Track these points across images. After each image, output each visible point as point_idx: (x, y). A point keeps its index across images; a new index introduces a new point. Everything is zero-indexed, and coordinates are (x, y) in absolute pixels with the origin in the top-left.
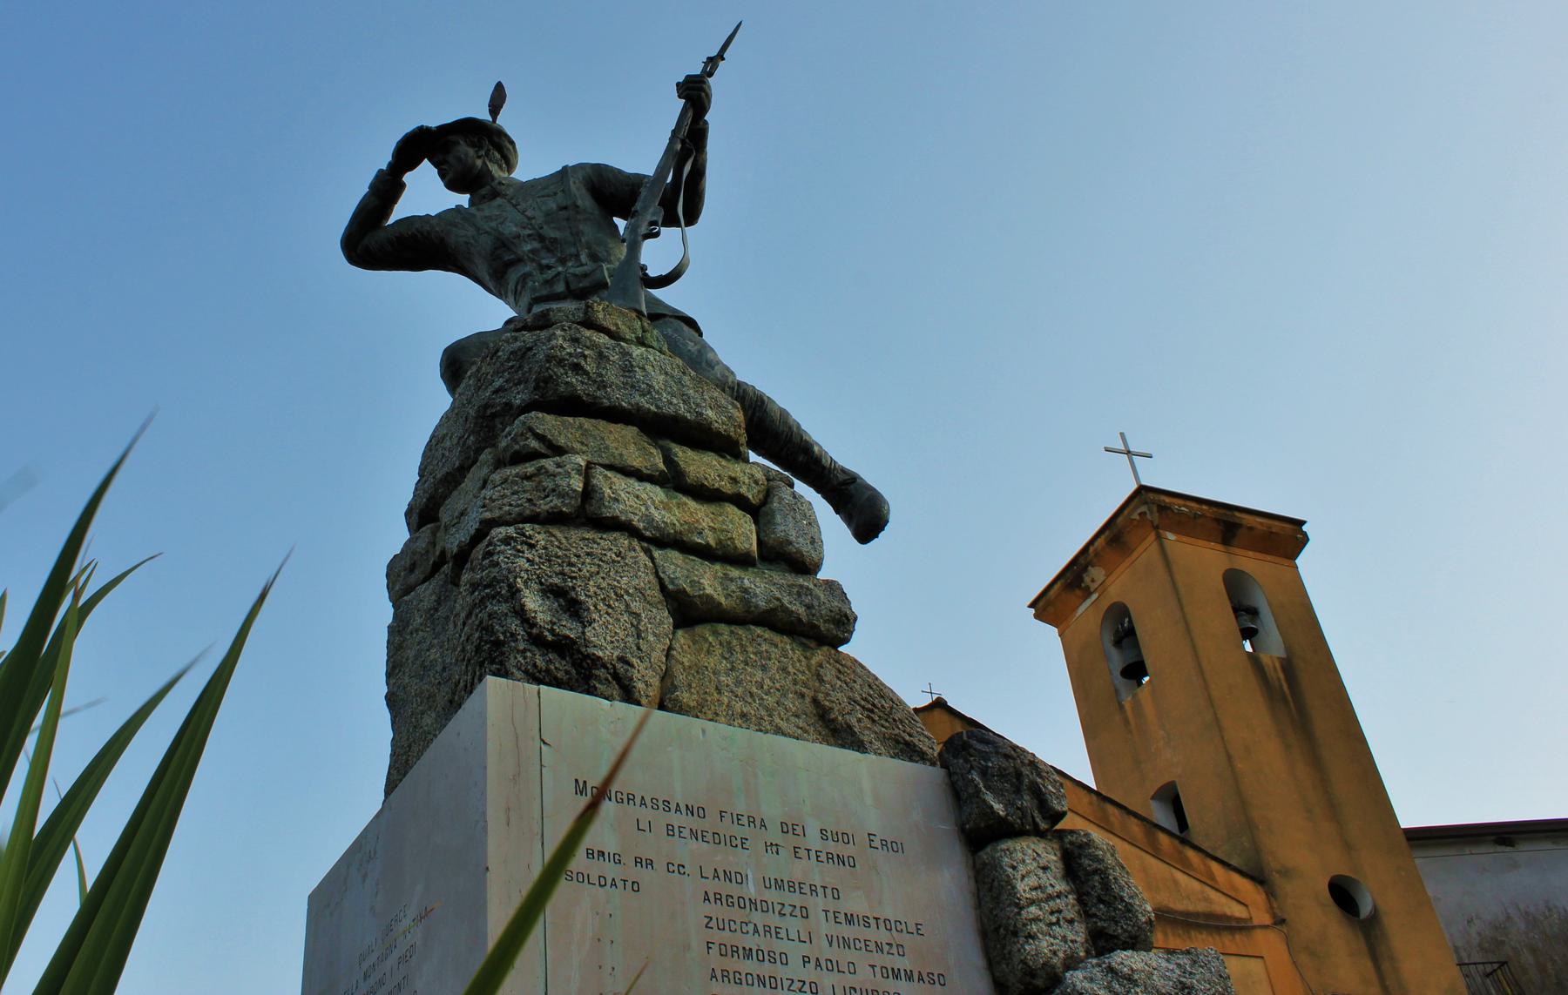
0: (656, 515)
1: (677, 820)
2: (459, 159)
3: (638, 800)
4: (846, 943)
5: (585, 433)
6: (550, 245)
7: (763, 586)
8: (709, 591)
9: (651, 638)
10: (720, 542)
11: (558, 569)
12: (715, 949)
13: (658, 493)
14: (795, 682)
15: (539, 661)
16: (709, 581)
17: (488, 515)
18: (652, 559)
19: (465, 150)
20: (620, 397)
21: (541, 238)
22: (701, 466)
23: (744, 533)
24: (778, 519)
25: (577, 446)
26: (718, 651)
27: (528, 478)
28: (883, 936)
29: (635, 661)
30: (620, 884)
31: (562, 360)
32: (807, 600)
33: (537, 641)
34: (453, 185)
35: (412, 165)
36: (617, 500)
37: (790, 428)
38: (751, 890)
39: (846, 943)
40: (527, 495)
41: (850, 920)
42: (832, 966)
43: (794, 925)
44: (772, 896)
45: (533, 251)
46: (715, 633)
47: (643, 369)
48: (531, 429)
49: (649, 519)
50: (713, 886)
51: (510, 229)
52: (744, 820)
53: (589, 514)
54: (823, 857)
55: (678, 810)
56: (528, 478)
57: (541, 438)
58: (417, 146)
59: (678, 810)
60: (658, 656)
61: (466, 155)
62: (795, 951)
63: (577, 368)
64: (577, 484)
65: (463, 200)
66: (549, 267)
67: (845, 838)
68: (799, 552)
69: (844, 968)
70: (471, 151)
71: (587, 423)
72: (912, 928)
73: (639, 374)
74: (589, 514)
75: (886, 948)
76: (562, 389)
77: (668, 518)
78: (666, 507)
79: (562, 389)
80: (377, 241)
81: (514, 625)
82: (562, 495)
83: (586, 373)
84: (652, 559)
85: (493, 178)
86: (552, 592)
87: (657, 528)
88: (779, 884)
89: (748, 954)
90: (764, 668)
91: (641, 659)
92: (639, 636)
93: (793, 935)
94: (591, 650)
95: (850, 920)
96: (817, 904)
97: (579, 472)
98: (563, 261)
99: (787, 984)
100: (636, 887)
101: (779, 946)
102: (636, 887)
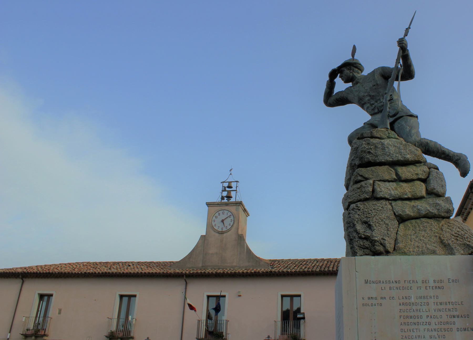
0: (393, 192)
1: (392, 285)
2: (346, 75)
3: (382, 282)
4: (440, 310)
5: (373, 171)
6: (372, 97)
7: (424, 206)
8: (408, 212)
9: (392, 230)
10: (412, 195)
11: (365, 216)
12: (402, 317)
13: (393, 185)
14: (434, 233)
15: (362, 243)
16: (407, 208)
17: (350, 201)
18: (392, 206)
19: (346, 71)
20: (382, 159)
21: (370, 96)
22: (405, 172)
23: (421, 189)
24: (432, 182)
25: (371, 176)
26: (411, 228)
27: (359, 188)
28: (451, 306)
29: (386, 238)
30: (377, 305)
31: (365, 151)
32: (438, 207)
33: (360, 238)
34: (346, 81)
35: (335, 77)
36: (381, 191)
37: (438, 149)
38: (413, 300)
39: (440, 310)
40: (359, 194)
41: (441, 304)
42: (435, 317)
43: (424, 308)
44: (419, 301)
45: (368, 100)
46: (411, 223)
47: (388, 148)
48: (358, 174)
49: (391, 195)
50: (401, 301)
51: (362, 94)
52: (411, 282)
53: (374, 197)
54: (434, 288)
55: (393, 282)
56: (359, 188)
57: (361, 176)
58: (333, 74)
59: (393, 282)
60: (393, 235)
61: (347, 73)
62: (424, 315)
63: (369, 152)
64: (371, 189)
65: (350, 84)
66: (373, 104)
67: (441, 281)
68: (437, 191)
69: (438, 317)
70: (348, 71)
71: (373, 168)
72: (460, 303)
73: (387, 150)
74: (374, 197)
75: (452, 310)
76: (366, 160)
77: (396, 192)
78: (396, 189)
79: (366, 160)
80: (333, 99)
81: (355, 234)
82: (367, 193)
83: (372, 153)
84: (392, 206)
85: (356, 78)
86: (364, 223)
87: (393, 197)
88: (421, 298)
89: (411, 317)
90: (425, 231)
91: (388, 237)
92: (388, 230)
93: (424, 310)
94: (374, 238)
95: (441, 304)
96: (431, 301)
97: (371, 185)
98: (376, 102)
99: (421, 323)
100: (381, 305)
101: (420, 314)
102: (381, 305)
